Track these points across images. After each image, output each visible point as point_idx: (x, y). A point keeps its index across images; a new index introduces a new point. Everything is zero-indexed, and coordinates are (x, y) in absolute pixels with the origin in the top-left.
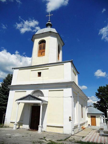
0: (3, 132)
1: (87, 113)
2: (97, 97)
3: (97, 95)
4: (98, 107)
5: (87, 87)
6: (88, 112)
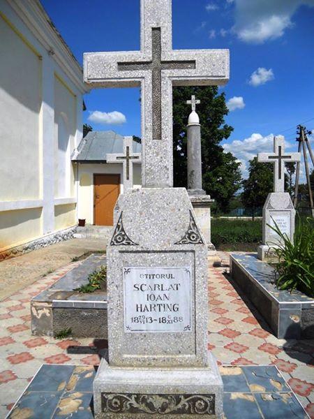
1: (73, 161)
5: (126, 117)
6: (77, 153)
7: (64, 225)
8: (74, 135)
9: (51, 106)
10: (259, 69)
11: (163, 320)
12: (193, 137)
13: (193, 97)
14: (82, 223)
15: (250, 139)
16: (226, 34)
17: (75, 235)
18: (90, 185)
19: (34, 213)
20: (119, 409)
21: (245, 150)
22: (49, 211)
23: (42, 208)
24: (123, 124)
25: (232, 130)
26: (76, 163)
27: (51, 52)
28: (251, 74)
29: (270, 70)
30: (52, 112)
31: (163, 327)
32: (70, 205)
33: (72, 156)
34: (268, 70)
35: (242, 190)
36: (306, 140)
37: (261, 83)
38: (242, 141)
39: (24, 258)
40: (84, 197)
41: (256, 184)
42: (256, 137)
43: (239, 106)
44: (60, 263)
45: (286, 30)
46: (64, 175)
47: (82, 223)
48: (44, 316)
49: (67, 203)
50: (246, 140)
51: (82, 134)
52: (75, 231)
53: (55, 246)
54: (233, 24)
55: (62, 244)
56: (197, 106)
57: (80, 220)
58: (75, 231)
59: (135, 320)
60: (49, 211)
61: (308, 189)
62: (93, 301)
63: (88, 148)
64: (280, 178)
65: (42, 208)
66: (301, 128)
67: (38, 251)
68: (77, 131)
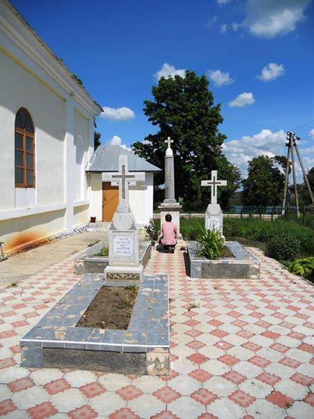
0: (44, 328)
1: (87, 172)
2: (150, 120)
3: (150, 110)
4: (149, 155)
5: (135, 113)
6: (89, 165)
7: (81, 221)
8: (87, 150)
9: (72, 134)
10: (270, 64)
11: (125, 252)
12: (168, 165)
13: (169, 138)
14: (93, 220)
15: (259, 135)
16: (238, 28)
17: (88, 229)
18: (99, 190)
19: (60, 213)
20: (111, 278)
21: (253, 147)
22: (70, 211)
23: (65, 209)
24: (132, 119)
25: (225, 138)
26: (89, 173)
27: (72, 95)
28: (261, 69)
29: (281, 65)
30: (72, 138)
31: (125, 254)
32: (84, 206)
33: (86, 167)
34: (279, 65)
35: (241, 189)
36: (295, 145)
37: (272, 78)
38: (251, 137)
39: (57, 244)
40: (94, 199)
41: (254, 184)
42: (266, 133)
43: (249, 103)
44: (81, 247)
45: (299, 25)
46: (79, 181)
47: (93, 220)
48: (81, 265)
49: (82, 204)
50: (255, 136)
51: (93, 149)
52: (88, 226)
53: (74, 237)
54: (245, 18)
55: (79, 236)
56: (171, 143)
57: (91, 218)
58: (88, 226)
59: (117, 252)
60: (70, 211)
61: (307, 188)
62: (103, 259)
63: (98, 160)
64: (214, 195)
65: (65, 209)
66: (291, 134)
67: (64, 240)
68: (90, 147)
